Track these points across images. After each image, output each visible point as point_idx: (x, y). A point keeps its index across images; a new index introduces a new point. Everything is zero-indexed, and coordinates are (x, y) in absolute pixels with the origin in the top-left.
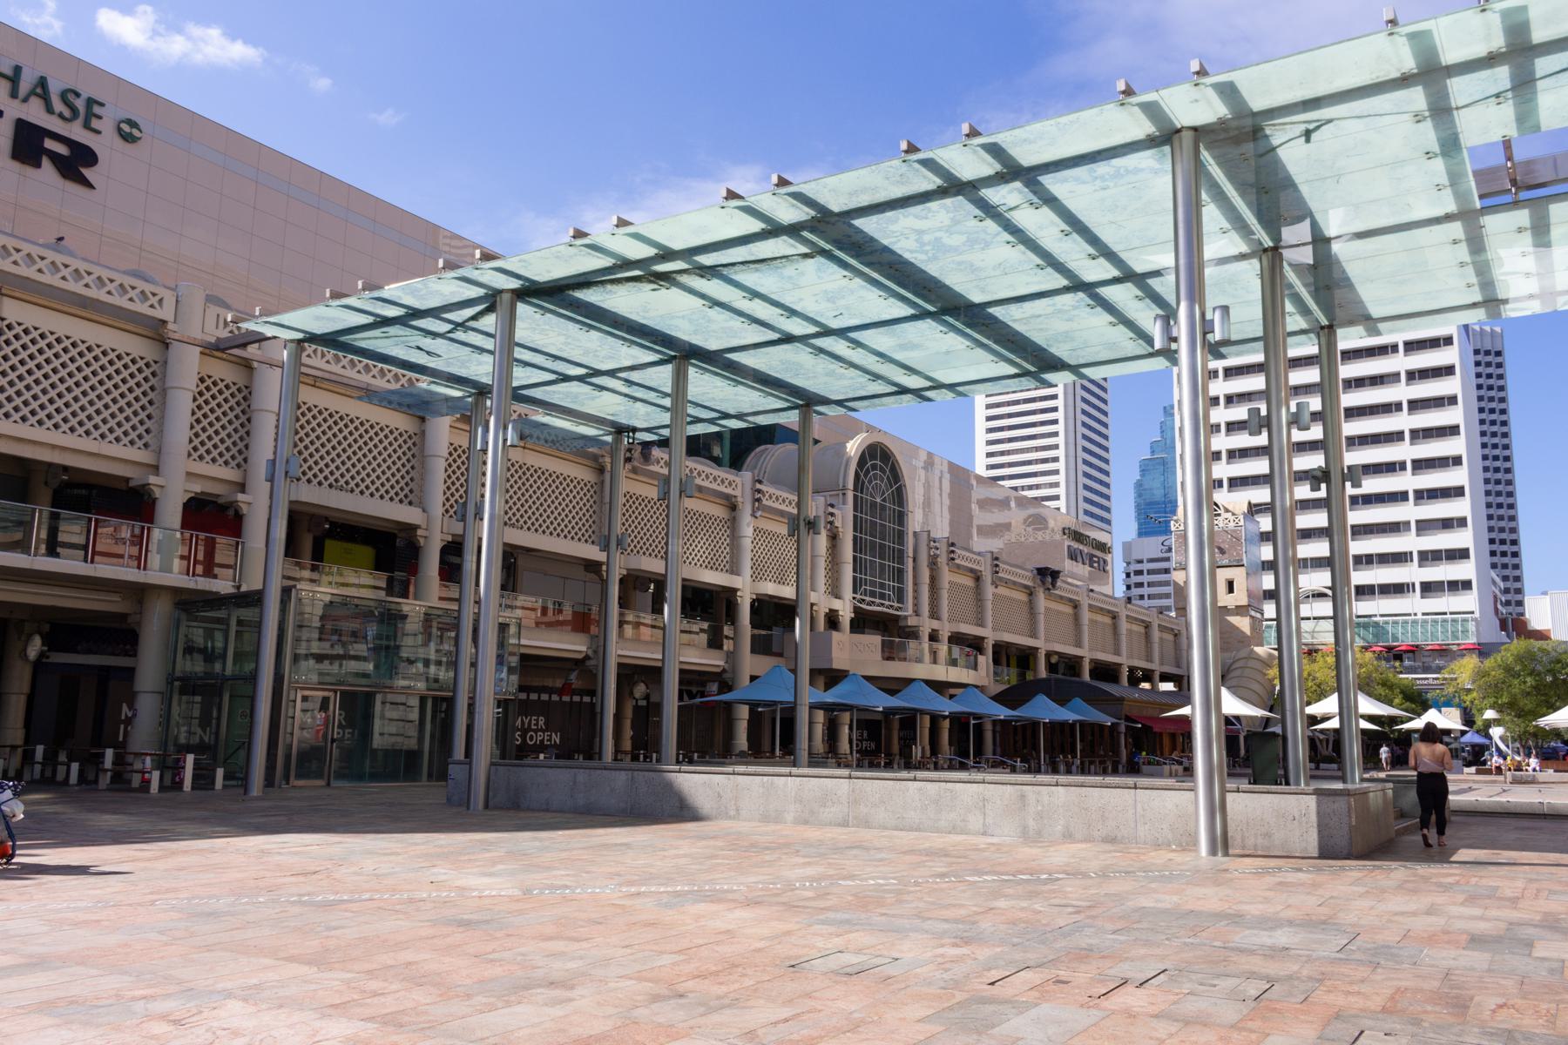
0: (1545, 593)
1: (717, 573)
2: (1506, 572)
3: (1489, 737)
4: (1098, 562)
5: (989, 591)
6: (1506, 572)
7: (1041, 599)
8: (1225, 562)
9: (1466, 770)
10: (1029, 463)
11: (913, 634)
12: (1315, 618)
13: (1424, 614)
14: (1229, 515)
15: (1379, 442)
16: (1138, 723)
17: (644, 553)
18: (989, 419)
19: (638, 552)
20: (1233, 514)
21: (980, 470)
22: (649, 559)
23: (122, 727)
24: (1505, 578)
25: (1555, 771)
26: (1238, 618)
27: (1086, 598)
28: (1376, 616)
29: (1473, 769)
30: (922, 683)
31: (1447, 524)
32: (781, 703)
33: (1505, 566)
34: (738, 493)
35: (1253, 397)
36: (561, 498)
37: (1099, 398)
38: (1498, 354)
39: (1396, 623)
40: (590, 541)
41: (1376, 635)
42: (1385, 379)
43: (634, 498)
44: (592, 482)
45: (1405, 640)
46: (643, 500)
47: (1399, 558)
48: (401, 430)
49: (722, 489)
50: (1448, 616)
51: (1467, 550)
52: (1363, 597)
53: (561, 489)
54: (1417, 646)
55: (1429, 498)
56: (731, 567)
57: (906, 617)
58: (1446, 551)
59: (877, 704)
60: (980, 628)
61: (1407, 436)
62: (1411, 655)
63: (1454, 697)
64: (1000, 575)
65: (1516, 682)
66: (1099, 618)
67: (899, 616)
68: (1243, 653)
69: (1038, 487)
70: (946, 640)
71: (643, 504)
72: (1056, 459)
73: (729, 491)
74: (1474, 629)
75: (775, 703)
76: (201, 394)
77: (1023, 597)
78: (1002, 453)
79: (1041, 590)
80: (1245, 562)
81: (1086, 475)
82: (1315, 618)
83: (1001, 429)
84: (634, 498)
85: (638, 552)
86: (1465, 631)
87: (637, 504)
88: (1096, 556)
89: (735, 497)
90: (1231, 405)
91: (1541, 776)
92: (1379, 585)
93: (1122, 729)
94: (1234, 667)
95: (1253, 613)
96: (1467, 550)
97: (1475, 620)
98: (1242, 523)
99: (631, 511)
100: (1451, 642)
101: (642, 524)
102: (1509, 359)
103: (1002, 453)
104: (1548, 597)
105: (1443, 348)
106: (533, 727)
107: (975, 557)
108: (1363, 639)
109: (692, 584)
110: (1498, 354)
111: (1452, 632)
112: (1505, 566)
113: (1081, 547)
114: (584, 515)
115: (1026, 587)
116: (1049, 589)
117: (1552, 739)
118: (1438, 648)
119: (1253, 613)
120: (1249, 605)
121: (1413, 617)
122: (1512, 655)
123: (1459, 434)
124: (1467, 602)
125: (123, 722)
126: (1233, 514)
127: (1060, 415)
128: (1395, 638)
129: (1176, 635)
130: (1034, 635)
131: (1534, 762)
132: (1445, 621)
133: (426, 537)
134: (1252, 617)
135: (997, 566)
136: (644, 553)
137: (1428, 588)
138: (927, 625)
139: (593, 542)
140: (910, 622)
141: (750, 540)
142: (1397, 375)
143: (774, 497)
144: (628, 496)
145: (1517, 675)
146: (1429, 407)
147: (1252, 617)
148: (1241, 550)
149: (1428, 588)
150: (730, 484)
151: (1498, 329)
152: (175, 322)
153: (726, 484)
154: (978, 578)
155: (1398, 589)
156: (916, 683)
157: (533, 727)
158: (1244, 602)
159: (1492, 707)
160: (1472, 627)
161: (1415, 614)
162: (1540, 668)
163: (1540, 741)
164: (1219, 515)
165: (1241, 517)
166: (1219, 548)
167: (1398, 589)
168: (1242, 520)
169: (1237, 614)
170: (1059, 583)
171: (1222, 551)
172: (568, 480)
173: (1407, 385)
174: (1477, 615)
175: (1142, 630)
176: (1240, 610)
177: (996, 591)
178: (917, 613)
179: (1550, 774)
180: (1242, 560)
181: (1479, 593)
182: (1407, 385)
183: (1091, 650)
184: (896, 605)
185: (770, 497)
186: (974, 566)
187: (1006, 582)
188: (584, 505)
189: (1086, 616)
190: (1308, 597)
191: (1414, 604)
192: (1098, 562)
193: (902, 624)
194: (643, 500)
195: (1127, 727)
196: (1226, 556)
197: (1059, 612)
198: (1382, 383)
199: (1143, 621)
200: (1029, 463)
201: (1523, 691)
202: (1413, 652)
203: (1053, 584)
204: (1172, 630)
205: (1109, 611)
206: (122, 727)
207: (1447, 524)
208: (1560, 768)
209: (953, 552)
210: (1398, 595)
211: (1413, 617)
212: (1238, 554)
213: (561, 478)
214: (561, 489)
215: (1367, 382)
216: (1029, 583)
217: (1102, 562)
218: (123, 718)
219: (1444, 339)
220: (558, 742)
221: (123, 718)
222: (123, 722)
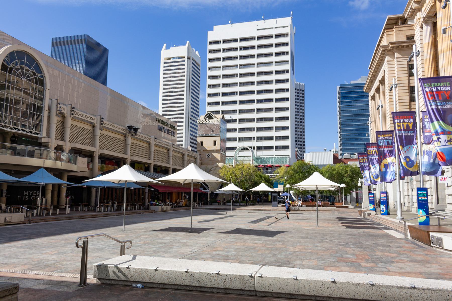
0: (309, 153)
1: (138, 158)
2: (302, 150)
3: (290, 193)
4: (171, 133)
5: (98, 132)
6: (302, 150)
7: (130, 140)
8: (214, 135)
9: (279, 205)
10: (175, 111)
11: (46, 146)
12: (244, 156)
13: (275, 156)
14: (216, 119)
15: (266, 102)
16: (152, 188)
17: (77, 143)
18: (163, 96)
19: (75, 142)
20: (217, 119)
21: (160, 113)
22: (106, 151)
23: (24, 196)
24: (301, 151)
25: (306, 206)
26: (217, 154)
27: (187, 153)
28: (261, 156)
29: (281, 205)
30: (44, 170)
31: (284, 128)
32: (101, 187)
33: (301, 148)
34: (95, 122)
35: (231, 85)
36: (75, 133)
37: (197, 93)
38: (303, 91)
39: (267, 158)
40: (90, 145)
41: (261, 162)
42: (269, 82)
43: (82, 128)
44: (91, 130)
45: (269, 164)
46: (81, 128)
47: (269, 138)
48: (90, 129)
49: (90, 120)
50: (282, 156)
51: (289, 136)
52: (259, 150)
53: (75, 131)
54: (273, 165)
55: (279, 120)
56: (93, 145)
57: (41, 138)
58: (283, 136)
59: (41, 182)
60: (126, 155)
61: (274, 100)
62: (271, 168)
63: (278, 180)
64: (104, 125)
65: (297, 175)
66: (178, 155)
67: (38, 137)
68: (215, 165)
69: (177, 118)
70: (53, 149)
71: (84, 130)
72: (183, 110)
73: (92, 121)
74: (289, 160)
75: (98, 187)
76: (71, 128)
77: (122, 138)
78: (167, 107)
79: (130, 135)
80: (220, 135)
81: (192, 116)
82: (244, 156)
83: (167, 100)
84: (82, 128)
85: (75, 142)
86: (286, 161)
87: (81, 129)
88: (170, 130)
89: (94, 123)
90: (223, 87)
91: (301, 208)
92: (263, 147)
93: (64, 188)
94: (212, 170)
95: (222, 153)
96: (289, 136)
97: (289, 158)
98: (220, 122)
99: (78, 133)
100: (282, 164)
101: (81, 136)
102: (306, 92)
103: (167, 107)
104: (310, 154)
105: (286, 74)
106: (34, 194)
107: (168, 144)
108: (257, 163)
109: (115, 157)
110: (303, 91)
111: (283, 161)
112: (301, 148)
113: (163, 126)
114: (88, 137)
115: (123, 134)
116: (132, 135)
117: (307, 194)
118: (278, 166)
119: (222, 153)
120: (221, 150)
121: (272, 156)
122: (296, 166)
123: (289, 101)
124: (287, 152)
125: (24, 195)
126: (217, 119)
127: (185, 97)
128: (266, 163)
129: (195, 159)
130: (169, 163)
131: (300, 203)
132: (281, 158)
133: (51, 145)
134: (221, 154)
135: (102, 121)
136: (77, 143)
137: (277, 148)
138: (53, 143)
139: (91, 146)
140: (43, 140)
141: (70, 128)
142: (273, 81)
143: (115, 127)
144: (58, 121)
145: (297, 173)
146: (281, 92)
147: (221, 154)
148: (219, 131)
149: (277, 148)
150: (93, 119)
151: (303, 84)
152: (67, 113)
153: (117, 128)
154: (94, 127)
155: (269, 148)
156: (40, 170)
157: (34, 194)
158: (219, 148)
159: (288, 184)
160: (288, 160)
161: (273, 156)
162: (305, 170)
163: (304, 195)
164: (213, 119)
165: (220, 120)
166: (212, 130)
167: (269, 148)
168: (220, 121)
169: (217, 153)
170: (138, 133)
171: (213, 131)
172: (78, 127)
173: (275, 84)
174: (290, 156)
175: (181, 156)
176: (218, 151)
177: (101, 132)
178: (48, 135)
179: (304, 208)
180: (219, 134)
181: (291, 150)
182: (275, 84)
183: (172, 165)
184: (34, 131)
185: (106, 124)
186: (148, 140)
187: (108, 129)
188: (89, 136)
189: (171, 153)
190: (242, 149)
191: (273, 153)
192: (171, 133)
193: (39, 141)
194: (88, 130)
195: (149, 190)
196: (214, 133)
197: (140, 146)
198: (268, 83)
199: (182, 153)
200: (175, 111)
201: (299, 178)
202: (271, 167)
203: (136, 134)
204: (194, 157)
205: (166, 148)
206: (24, 196)
207: (284, 128)
208: (308, 205)
209: (73, 111)
210: (269, 150)
211: (272, 156)
212: (218, 132)
213: (78, 127)
214: (75, 131)
215: (264, 83)
216: (125, 132)
217: (172, 133)
218: (24, 194)
219: (286, 71)
220: (74, 198)
221: (24, 194)
222: (24, 195)
